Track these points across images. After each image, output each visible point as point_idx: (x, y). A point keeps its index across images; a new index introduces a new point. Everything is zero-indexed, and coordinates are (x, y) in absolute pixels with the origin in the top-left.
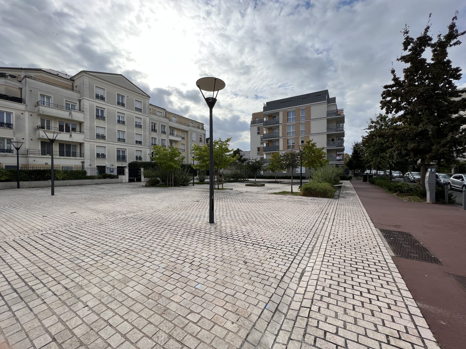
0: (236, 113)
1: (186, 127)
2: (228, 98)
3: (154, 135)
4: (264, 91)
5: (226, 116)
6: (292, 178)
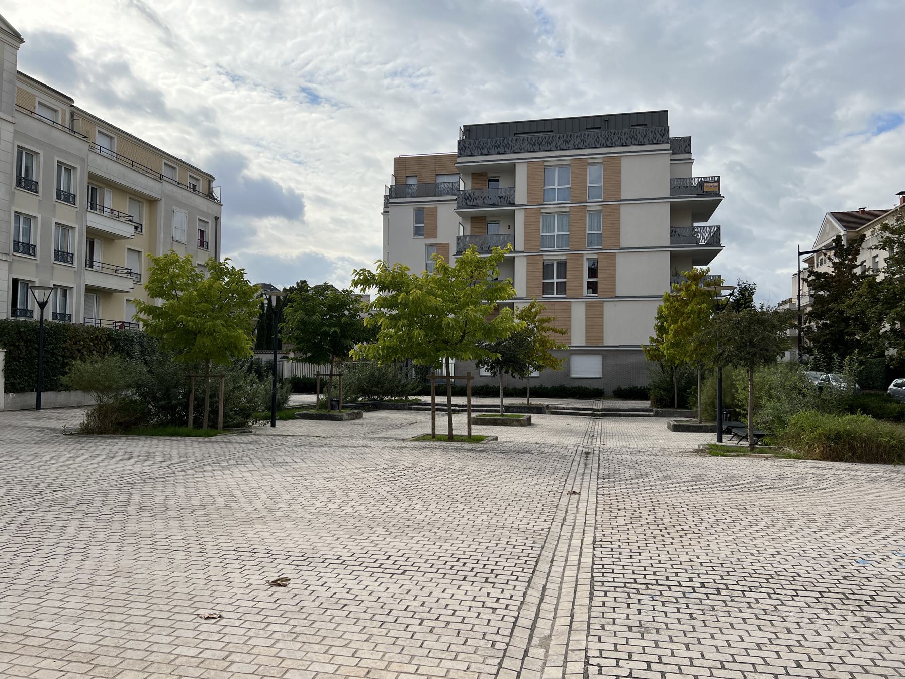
0: (231, 146)
1: (151, 183)
2: (205, 85)
3: (26, 203)
4: (339, 80)
5: (190, 151)
6: (501, 394)
